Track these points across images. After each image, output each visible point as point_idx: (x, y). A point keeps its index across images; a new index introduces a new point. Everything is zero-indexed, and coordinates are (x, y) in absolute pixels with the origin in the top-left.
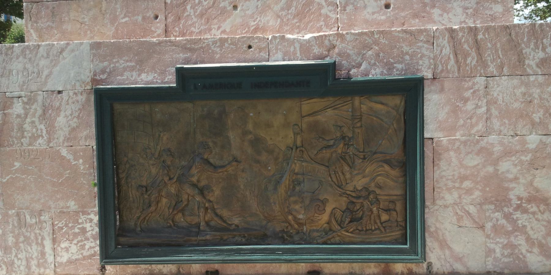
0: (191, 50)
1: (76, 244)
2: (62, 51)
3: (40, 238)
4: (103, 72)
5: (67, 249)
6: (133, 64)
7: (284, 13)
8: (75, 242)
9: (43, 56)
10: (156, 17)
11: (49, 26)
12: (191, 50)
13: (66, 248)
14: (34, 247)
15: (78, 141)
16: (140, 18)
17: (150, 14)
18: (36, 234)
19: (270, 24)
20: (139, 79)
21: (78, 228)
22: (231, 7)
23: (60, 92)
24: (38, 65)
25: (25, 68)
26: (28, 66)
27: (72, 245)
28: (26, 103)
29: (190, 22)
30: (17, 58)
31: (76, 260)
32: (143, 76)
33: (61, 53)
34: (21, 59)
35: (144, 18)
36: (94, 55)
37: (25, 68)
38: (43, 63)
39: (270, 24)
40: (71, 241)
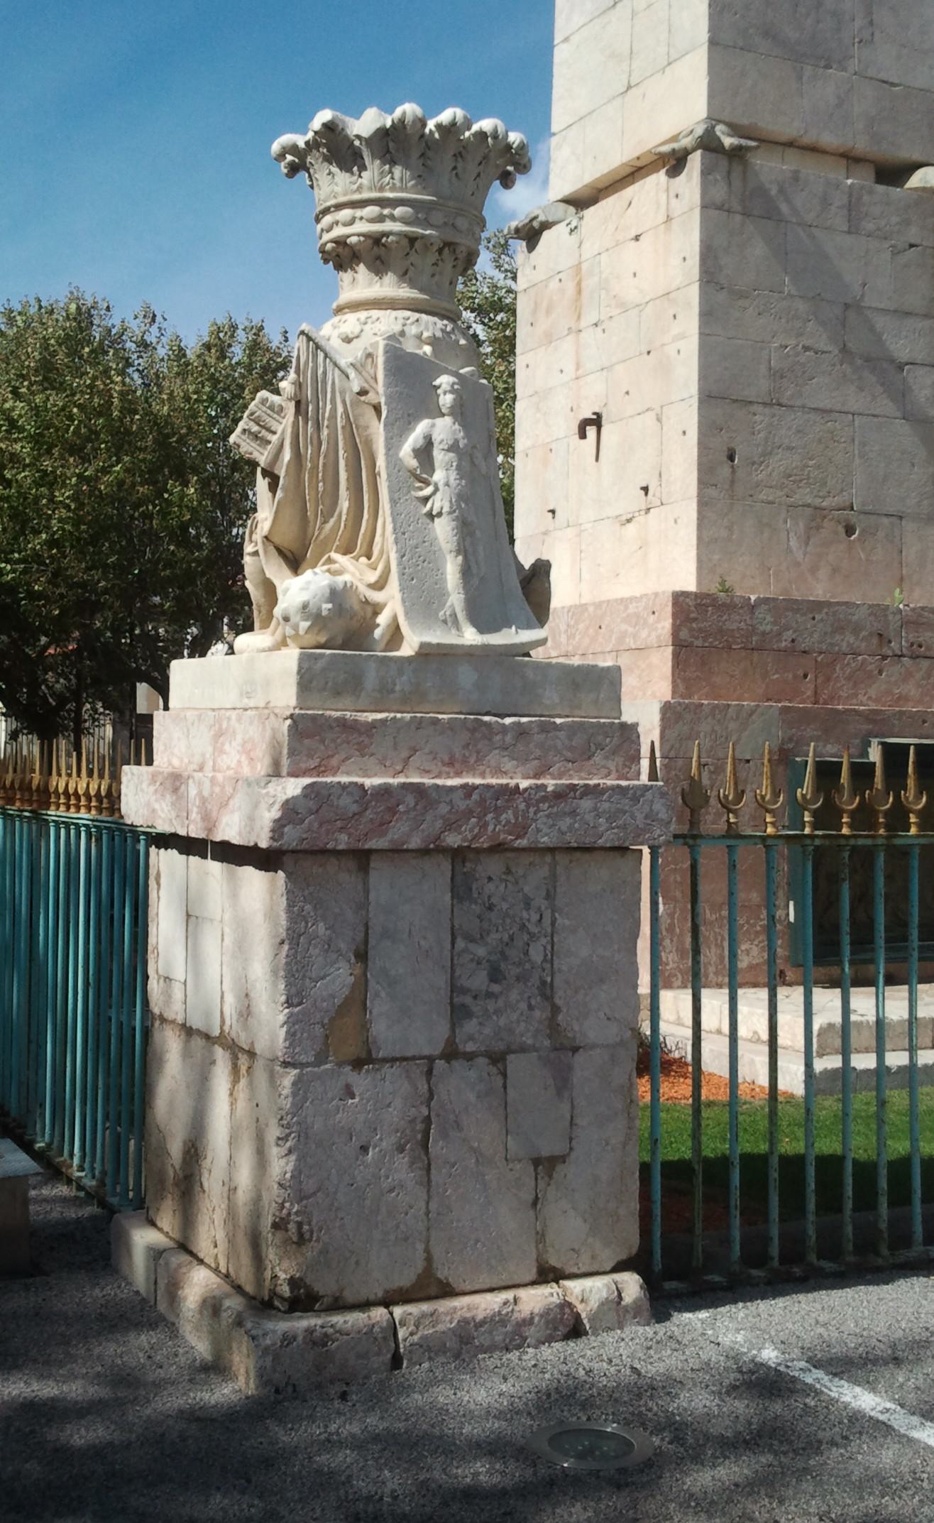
0: (874, 722)
1: (757, 946)
2: (752, 713)
3: (720, 938)
4: (791, 740)
5: (748, 952)
6: (820, 733)
7: (924, 682)
8: (756, 942)
9: (732, 718)
10: (805, 676)
11: (697, 676)
12: (874, 722)
13: (747, 950)
14: (713, 949)
15: (278, 478)
16: (791, 676)
17: (801, 673)
18: (715, 932)
19: (912, 693)
20: (824, 752)
21: (761, 926)
22: (876, 672)
23: (748, 761)
24: (727, 728)
25: (713, 730)
26: (717, 728)
27: (753, 946)
28: (713, 772)
29: (839, 685)
30: (706, 718)
31: (757, 964)
32: (829, 747)
33: (751, 715)
34: (709, 719)
35: (795, 677)
36: (783, 721)
37: (713, 730)
38: (732, 726)
39: (912, 693)
40: (752, 941)
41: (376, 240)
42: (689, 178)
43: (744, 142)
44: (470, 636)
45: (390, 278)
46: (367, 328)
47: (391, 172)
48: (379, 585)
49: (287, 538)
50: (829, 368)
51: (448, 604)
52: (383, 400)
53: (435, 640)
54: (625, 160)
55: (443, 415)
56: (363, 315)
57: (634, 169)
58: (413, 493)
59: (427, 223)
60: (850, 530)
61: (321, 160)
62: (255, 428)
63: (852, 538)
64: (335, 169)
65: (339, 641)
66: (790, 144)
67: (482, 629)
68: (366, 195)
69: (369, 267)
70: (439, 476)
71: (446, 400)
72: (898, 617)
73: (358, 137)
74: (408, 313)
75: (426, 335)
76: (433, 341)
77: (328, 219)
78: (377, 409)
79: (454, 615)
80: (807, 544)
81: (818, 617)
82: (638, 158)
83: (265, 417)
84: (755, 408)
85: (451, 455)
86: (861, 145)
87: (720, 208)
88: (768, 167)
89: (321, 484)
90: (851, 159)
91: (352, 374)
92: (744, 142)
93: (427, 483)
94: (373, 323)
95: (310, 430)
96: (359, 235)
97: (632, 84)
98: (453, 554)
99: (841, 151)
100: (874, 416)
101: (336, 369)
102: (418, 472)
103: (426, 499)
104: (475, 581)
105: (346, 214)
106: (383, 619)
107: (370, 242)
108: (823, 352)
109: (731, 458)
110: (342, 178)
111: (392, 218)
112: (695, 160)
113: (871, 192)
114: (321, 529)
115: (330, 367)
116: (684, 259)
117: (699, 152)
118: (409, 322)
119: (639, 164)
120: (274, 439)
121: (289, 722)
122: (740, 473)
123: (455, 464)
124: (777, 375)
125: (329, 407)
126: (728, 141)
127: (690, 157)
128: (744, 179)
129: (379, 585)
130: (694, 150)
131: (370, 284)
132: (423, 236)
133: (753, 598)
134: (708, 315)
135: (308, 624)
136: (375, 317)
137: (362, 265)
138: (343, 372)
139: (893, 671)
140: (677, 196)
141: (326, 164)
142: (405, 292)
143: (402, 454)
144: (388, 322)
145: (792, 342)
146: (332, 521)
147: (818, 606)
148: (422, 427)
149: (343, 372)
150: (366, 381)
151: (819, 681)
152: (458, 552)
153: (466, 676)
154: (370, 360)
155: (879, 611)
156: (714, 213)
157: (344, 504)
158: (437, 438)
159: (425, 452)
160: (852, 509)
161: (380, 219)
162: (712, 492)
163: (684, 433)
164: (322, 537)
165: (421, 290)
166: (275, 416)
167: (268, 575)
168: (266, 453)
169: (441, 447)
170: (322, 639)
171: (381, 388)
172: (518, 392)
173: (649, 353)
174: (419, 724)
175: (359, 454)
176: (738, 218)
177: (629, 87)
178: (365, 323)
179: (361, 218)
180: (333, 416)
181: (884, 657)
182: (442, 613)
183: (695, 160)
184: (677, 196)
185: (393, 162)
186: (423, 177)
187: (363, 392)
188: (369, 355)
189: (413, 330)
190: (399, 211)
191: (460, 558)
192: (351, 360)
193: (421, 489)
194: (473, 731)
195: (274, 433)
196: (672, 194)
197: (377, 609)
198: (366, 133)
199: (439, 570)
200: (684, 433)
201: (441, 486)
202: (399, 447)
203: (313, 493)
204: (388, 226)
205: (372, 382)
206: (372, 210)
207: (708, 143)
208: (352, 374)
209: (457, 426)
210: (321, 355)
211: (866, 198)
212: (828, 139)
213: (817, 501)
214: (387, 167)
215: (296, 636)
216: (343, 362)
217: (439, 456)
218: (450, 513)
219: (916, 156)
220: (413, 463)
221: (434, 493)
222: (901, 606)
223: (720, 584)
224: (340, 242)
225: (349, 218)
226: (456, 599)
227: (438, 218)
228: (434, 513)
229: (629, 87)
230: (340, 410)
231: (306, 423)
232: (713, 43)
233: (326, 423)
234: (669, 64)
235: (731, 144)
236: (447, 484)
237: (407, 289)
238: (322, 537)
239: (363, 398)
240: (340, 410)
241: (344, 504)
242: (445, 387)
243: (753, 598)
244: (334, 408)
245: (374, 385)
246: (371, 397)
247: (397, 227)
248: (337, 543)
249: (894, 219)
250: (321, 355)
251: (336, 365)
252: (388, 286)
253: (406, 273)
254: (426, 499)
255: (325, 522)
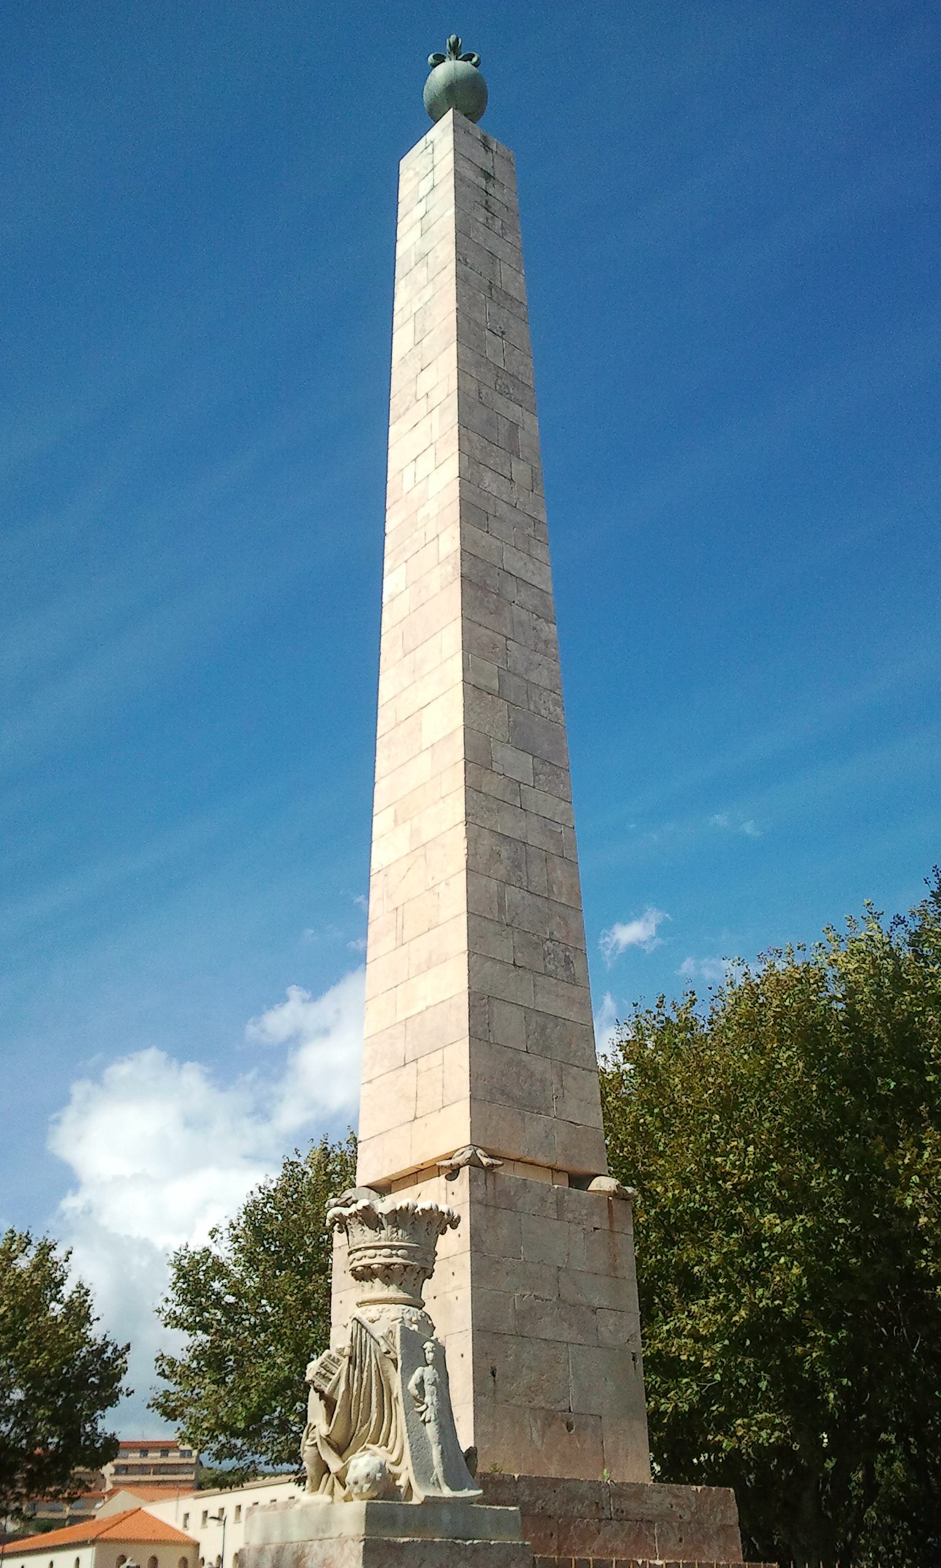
10: (552, 1535)
17: (548, 1532)
35: (545, 1535)
41: (388, 1266)
42: (461, 1183)
43: (495, 1162)
44: (447, 1492)
45: (393, 1287)
46: (383, 1315)
47: (397, 1231)
48: (397, 1463)
49: (337, 1437)
50: (551, 1311)
51: (434, 1473)
52: (399, 1357)
53: (432, 1495)
54: (413, 1165)
55: (428, 1365)
56: (380, 1307)
57: (417, 1170)
58: (415, 1409)
59: (413, 1258)
60: (569, 1427)
61: (357, 1223)
62: (324, 1372)
63: (571, 1433)
64: (366, 1228)
65: (381, 1495)
66: (518, 1161)
67: (453, 1489)
68: (383, 1243)
69: (383, 1282)
70: (428, 1399)
71: (430, 1356)
72: (607, 1490)
73: (381, 1213)
74: (404, 1307)
75: (414, 1319)
76: (417, 1322)
77: (359, 1254)
78: (395, 1362)
79: (437, 1480)
80: (543, 1437)
81: (558, 1490)
82: (422, 1164)
83: (329, 1365)
84: (506, 1338)
85: (434, 1387)
86: (560, 1164)
87: (480, 1203)
88: (510, 1174)
89: (361, 1404)
90: (554, 1170)
91: (382, 1342)
92: (495, 1162)
93: (423, 1404)
94: (386, 1312)
95: (356, 1372)
96: (379, 1264)
97: (418, 1116)
98: (437, 1444)
99: (548, 1165)
100: (580, 1344)
101: (372, 1339)
102: (418, 1397)
103: (422, 1413)
104: (446, 1460)
105: (371, 1252)
106: (401, 1482)
107: (384, 1267)
108: (547, 1300)
109: (494, 1375)
110: (369, 1233)
111: (397, 1255)
112: (465, 1172)
113: (569, 1194)
114: (359, 1430)
115: (369, 1337)
116: (459, 1235)
117: (467, 1167)
118: (405, 1312)
119: (422, 1167)
120: (334, 1378)
121: (363, 1543)
122: (499, 1383)
123: (435, 1392)
124: (518, 1315)
125: (368, 1360)
126: (485, 1161)
127: (461, 1169)
128: (495, 1183)
129: (397, 1463)
130: (465, 1165)
131: (382, 1289)
132: (412, 1265)
133: (516, 1476)
134: (476, 1274)
135: (368, 1485)
136: (387, 1309)
137: (377, 1279)
138: (375, 1340)
139: (607, 1530)
140: (453, 1193)
141: (360, 1225)
142: (401, 1295)
143: (409, 1387)
144: (395, 1310)
145: (528, 1293)
146: (366, 1425)
147: (557, 1481)
148: (419, 1371)
149: (375, 1340)
150: (389, 1346)
151: (561, 1538)
152: (439, 1443)
153: (446, 1516)
154: (391, 1334)
155: (596, 1486)
156: (477, 1206)
157: (374, 1416)
158: (426, 1378)
159: (420, 1385)
160: (570, 1411)
161: (391, 1256)
162: (483, 1399)
163: (462, 1355)
164: (360, 1434)
165: (410, 1294)
166: (335, 1364)
167: (324, 1458)
168: (329, 1386)
169: (429, 1382)
170: (375, 1494)
171: (398, 1351)
172: (332, 1321)
173: (435, 1297)
174: (424, 1544)
175: (384, 1388)
176: (492, 1210)
177: (416, 1118)
178: (382, 1312)
179: (380, 1255)
180: (370, 1365)
181: (601, 1520)
182: (431, 1479)
183: (465, 1172)
184: (453, 1193)
185: (398, 1227)
186: (412, 1235)
187: (388, 1352)
188: (391, 1332)
189: (407, 1316)
190: (400, 1252)
191: (440, 1447)
192: (381, 1334)
193: (419, 1407)
194: (451, 1548)
195: (334, 1374)
196: (450, 1192)
197: (396, 1477)
198: (385, 1212)
199: (429, 1453)
200: (462, 1355)
201: (429, 1405)
202: (408, 1383)
203: (357, 1408)
204: (395, 1260)
205: (392, 1346)
206: (387, 1251)
207: (473, 1162)
208: (382, 1342)
209: (435, 1371)
210: (364, 1331)
211: (566, 1197)
212: (541, 1159)
213: (548, 1406)
214: (395, 1229)
215: (360, 1494)
216: (376, 1336)
217: (428, 1388)
218: (435, 1420)
219: (593, 1170)
220: (416, 1392)
221: (426, 1409)
222: (609, 1482)
223: (492, 1466)
224: (368, 1267)
225: (373, 1255)
226: (438, 1471)
227: (419, 1255)
228: (426, 1420)
229: (416, 1118)
230: (374, 1362)
231: (355, 1369)
232: (472, 1098)
233: (366, 1369)
234: (444, 1107)
235: (487, 1163)
236: (432, 1404)
237: (402, 1293)
238: (360, 1434)
239: (387, 1355)
240: (374, 1362)
241: (374, 1416)
242: (429, 1349)
243: (516, 1476)
244: (371, 1361)
245: (394, 1349)
246: (392, 1355)
247: (400, 1260)
248: (368, 1438)
249: (584, 1212)
250: (364, 1331)
251: (372, 1336)
252: (392, 1292)
253: (401, 1284)
254: (422, 1413)
255: (362, 1426)
